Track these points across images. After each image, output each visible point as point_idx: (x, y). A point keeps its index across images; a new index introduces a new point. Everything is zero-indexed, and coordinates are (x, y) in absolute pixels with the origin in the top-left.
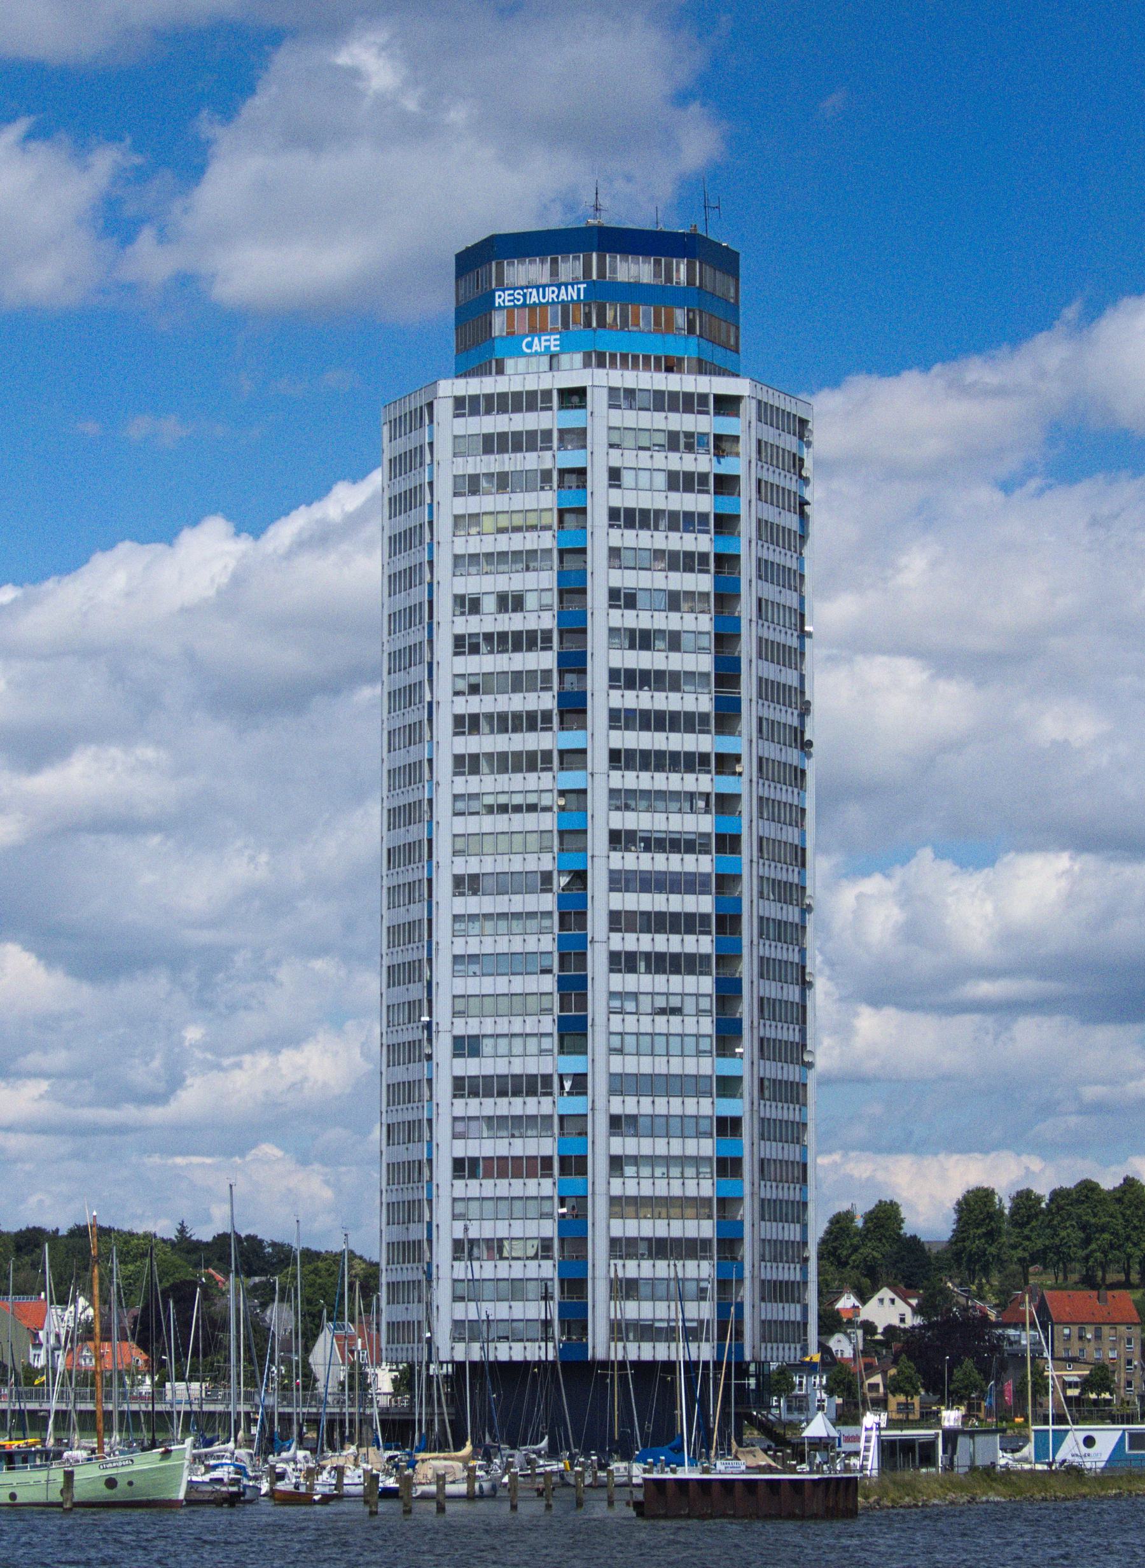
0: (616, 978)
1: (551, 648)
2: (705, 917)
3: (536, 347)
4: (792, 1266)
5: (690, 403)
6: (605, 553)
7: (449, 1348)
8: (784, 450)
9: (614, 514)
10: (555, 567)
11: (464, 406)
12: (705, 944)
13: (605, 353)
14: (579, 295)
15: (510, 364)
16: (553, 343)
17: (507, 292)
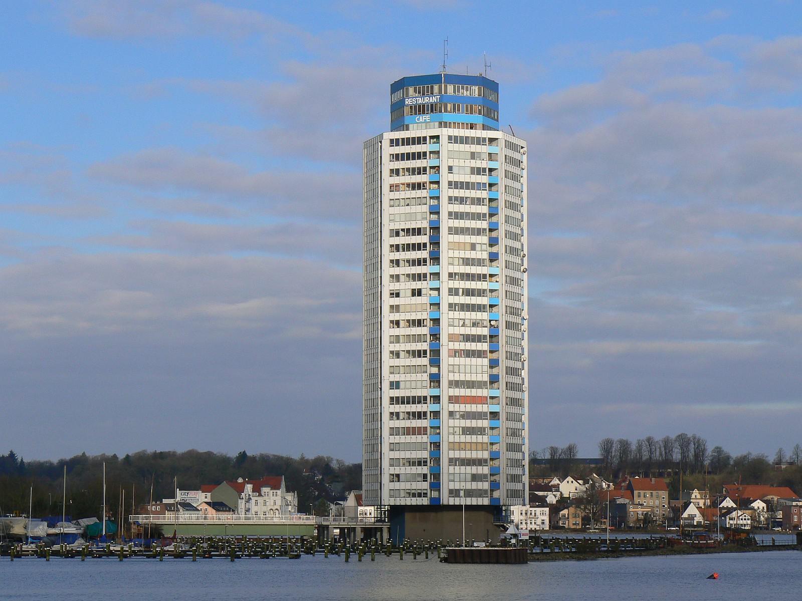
0: (451, 359)
1: (426, 357)
2: (485, 336)
3: (421, 120)
4: (519, 468)
5: (479, 141)
6: (447, 198)
7: (388, 500)
8: (513, 217)
9: (450, 183)
10: (428, 234)
11: (394, 142)
12: (485, 346)
13: (447, 122)
14: (437, 101)
15: (411, 126)
16: (427, 118)
17: (410, 99)
